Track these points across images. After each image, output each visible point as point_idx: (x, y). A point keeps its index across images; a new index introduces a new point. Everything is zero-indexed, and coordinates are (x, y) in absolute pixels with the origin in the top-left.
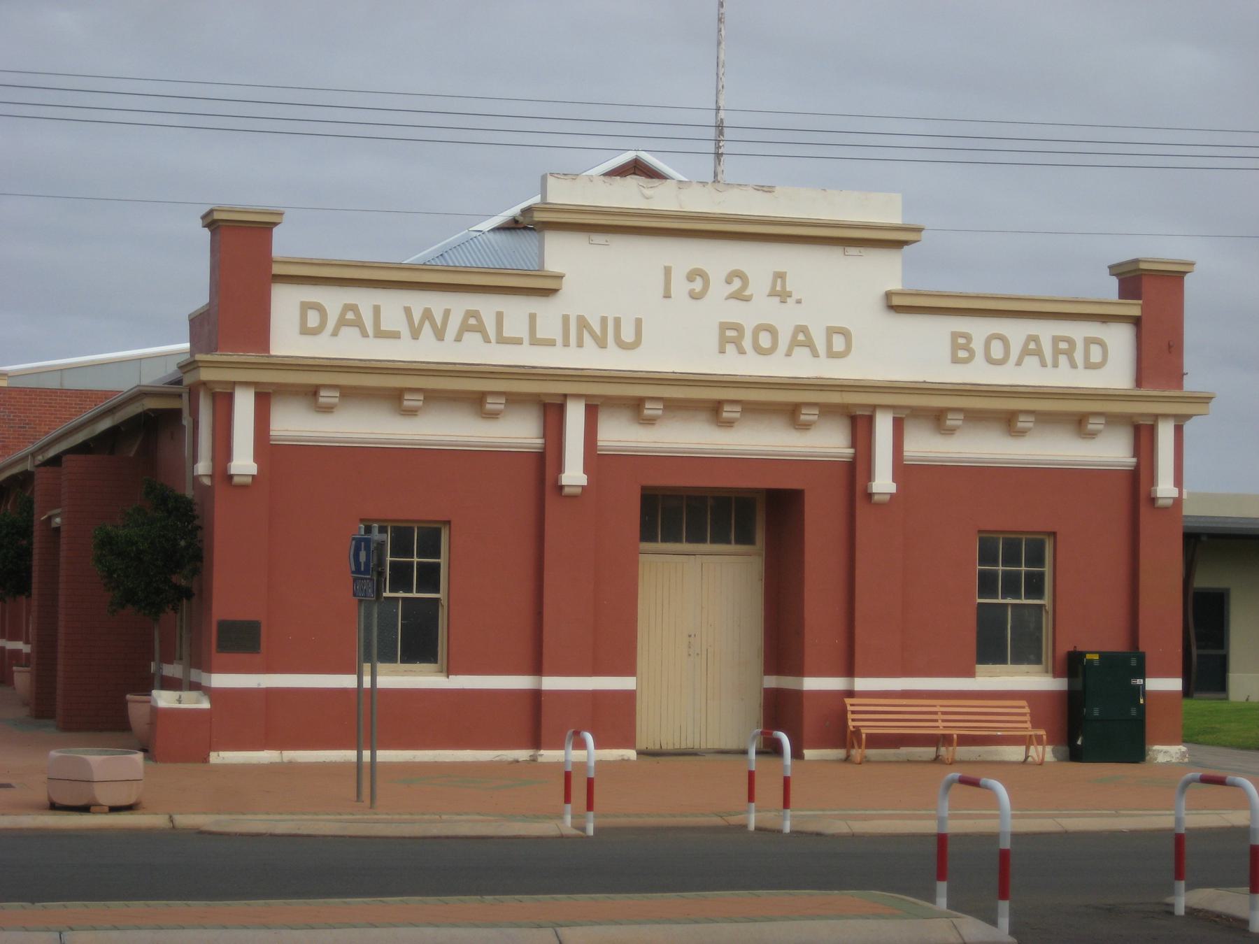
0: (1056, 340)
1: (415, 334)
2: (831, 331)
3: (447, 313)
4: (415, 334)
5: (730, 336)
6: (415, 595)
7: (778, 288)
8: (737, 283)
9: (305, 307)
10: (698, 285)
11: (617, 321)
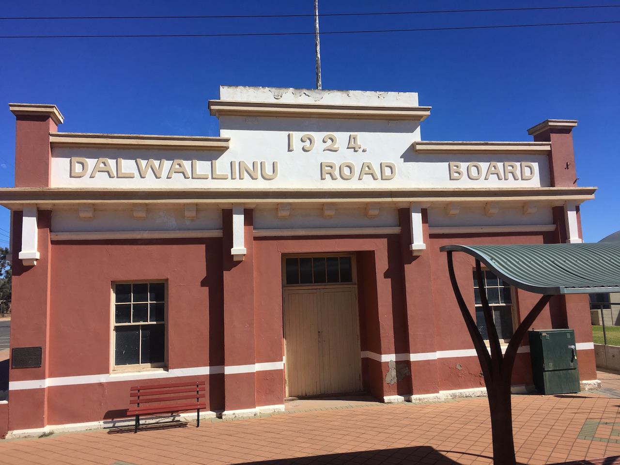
5: (325, 170)
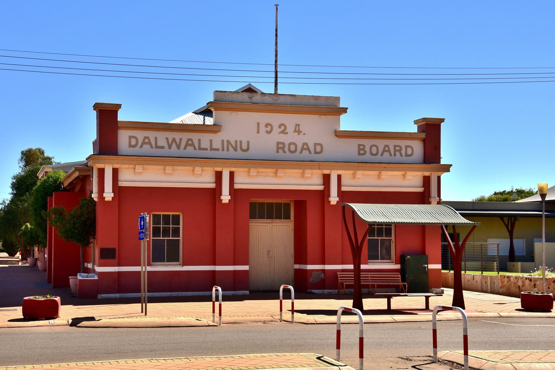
0: (395, 146)
1: (170, 147)
2: (316, 144)
3: (181, 139)
4: (170, 147)
6: (171, 238)
7: (297, 129)
8: (283, 128)
9: (130, 137)
10: (269, 129)
11: (241, 142)
